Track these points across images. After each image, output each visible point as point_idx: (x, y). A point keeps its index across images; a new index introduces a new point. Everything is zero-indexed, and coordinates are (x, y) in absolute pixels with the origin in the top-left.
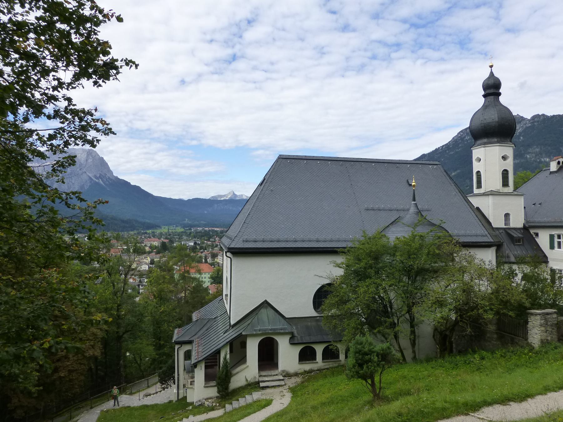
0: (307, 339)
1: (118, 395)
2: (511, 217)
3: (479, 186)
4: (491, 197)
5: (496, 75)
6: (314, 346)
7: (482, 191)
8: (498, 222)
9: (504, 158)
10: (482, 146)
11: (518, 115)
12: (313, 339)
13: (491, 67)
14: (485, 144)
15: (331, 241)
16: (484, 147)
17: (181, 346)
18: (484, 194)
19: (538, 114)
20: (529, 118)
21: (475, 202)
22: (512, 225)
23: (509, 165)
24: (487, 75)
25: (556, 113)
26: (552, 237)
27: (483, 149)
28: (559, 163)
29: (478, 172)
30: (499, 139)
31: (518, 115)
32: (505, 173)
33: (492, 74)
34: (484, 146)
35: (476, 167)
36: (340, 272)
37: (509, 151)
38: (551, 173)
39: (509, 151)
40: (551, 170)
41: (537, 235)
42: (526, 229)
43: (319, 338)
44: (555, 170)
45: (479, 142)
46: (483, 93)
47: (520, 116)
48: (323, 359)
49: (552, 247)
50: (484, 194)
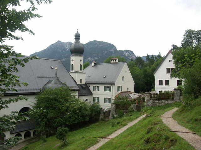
0: (18, 131)
1: (113, 112)
2: (82, 80)
3: (73, 69)
4: (76, 74)
6: (21, 133)
7: (73, 71)
8: (79, 82)
9: (81, 60)
11: (190, 34)
12: (21, 130)
13: (78, 29)
14: (75, 55)
15: (26, 90)
18: (75, 72)
21: (72, 75)
22: (82, 83)
23: (82, 63)
24: (76, 32)
26: (94, 87)
27: (74, 57)
28: (94, 63)
29: (72, 65)
30: (75, 54)
32: (81, 65)
35: (72, 63)
36: (175, 67)
37: (82, 58)
38: (92, 66)
39: (82, 58)
41: (89, 86)
42: (86, 84)
43: (23, 129)
45: (73, 54)
46: (75, 38)
49: (94, 90)
50: (75, 72)
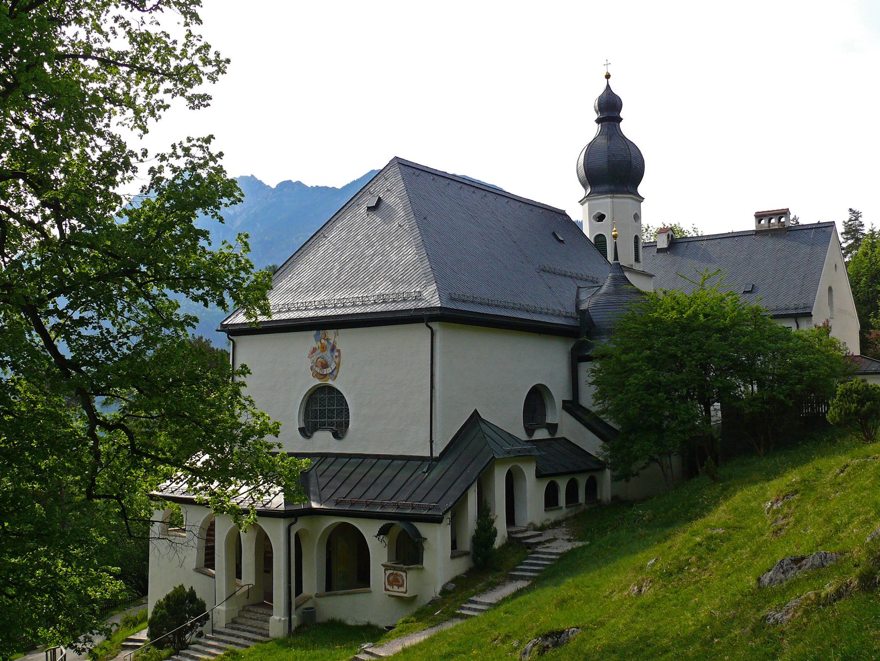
5: (615, 90)
10: (609, 195)
11: (252, 176)
16: (611, 198)
17: (296, 521)
19: (291, 181)
20: (273, 186)
24: (600, 90)
25: (321, 184)
27: (609, 200)
30: (612, 187)
31: (252, 176)
33: (608, 86)
34: (612, 195)
40: (658, 247)
44: (665, 246)
47: (256, 179)
48: (567, 502)
